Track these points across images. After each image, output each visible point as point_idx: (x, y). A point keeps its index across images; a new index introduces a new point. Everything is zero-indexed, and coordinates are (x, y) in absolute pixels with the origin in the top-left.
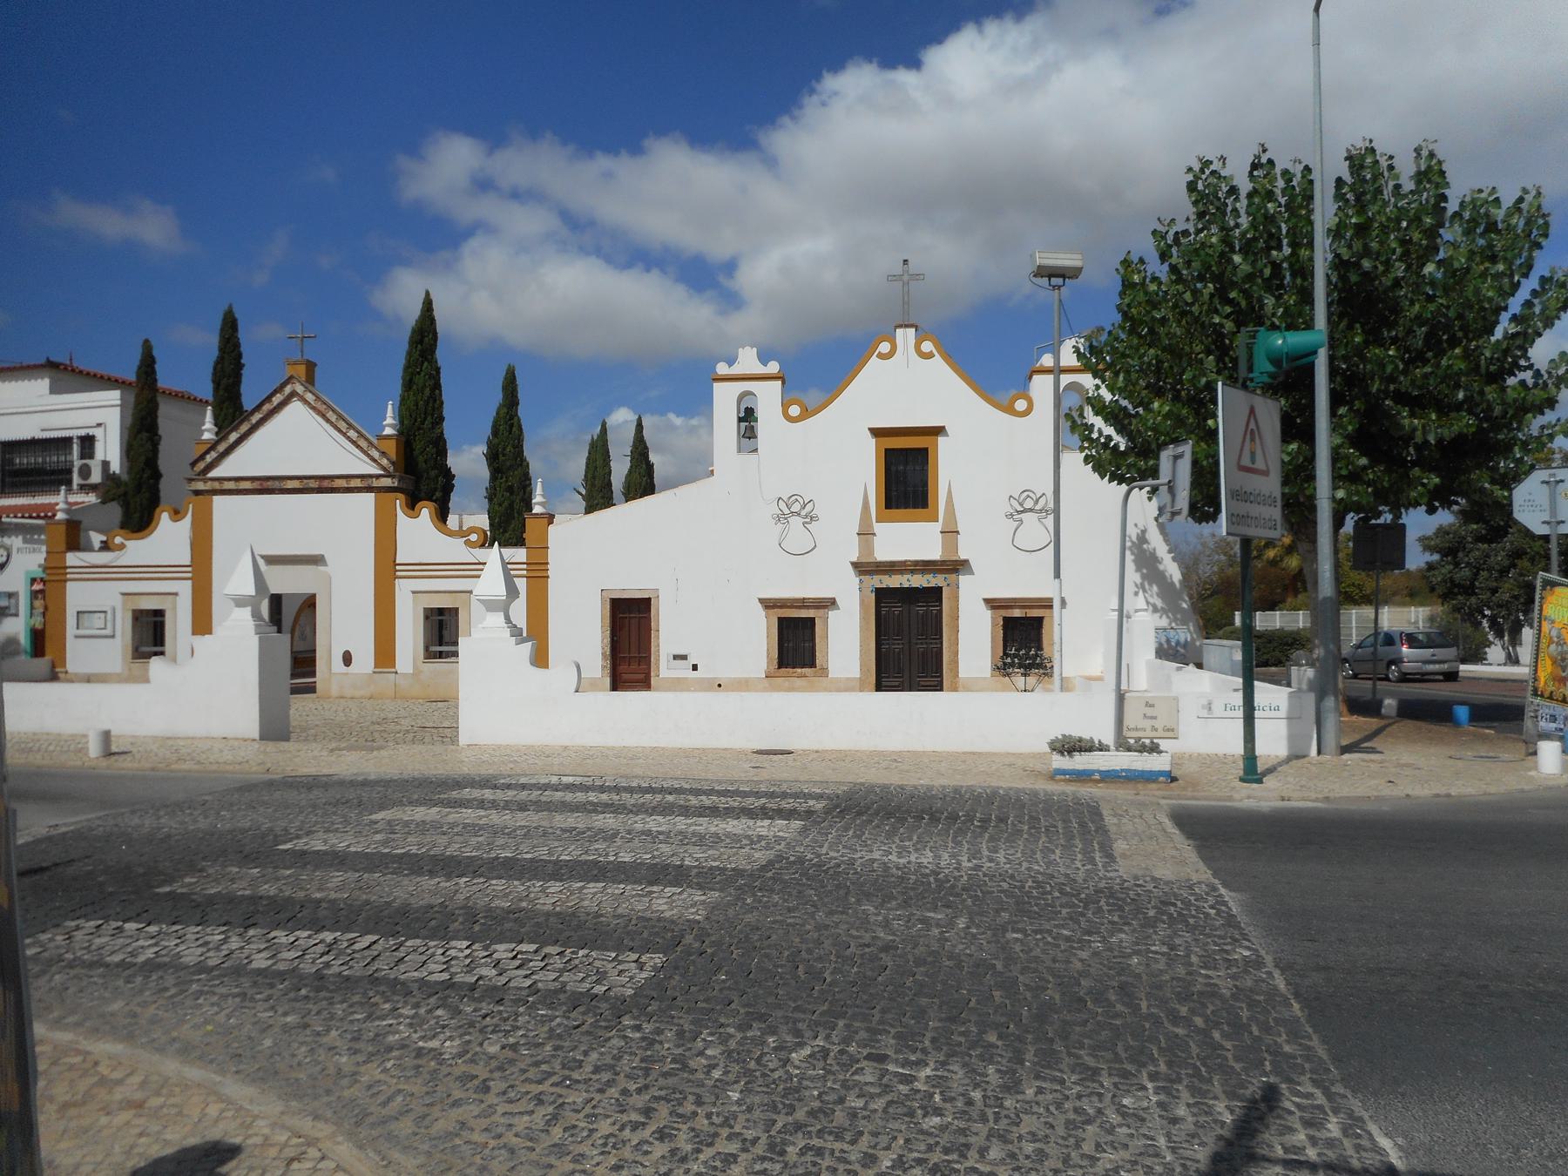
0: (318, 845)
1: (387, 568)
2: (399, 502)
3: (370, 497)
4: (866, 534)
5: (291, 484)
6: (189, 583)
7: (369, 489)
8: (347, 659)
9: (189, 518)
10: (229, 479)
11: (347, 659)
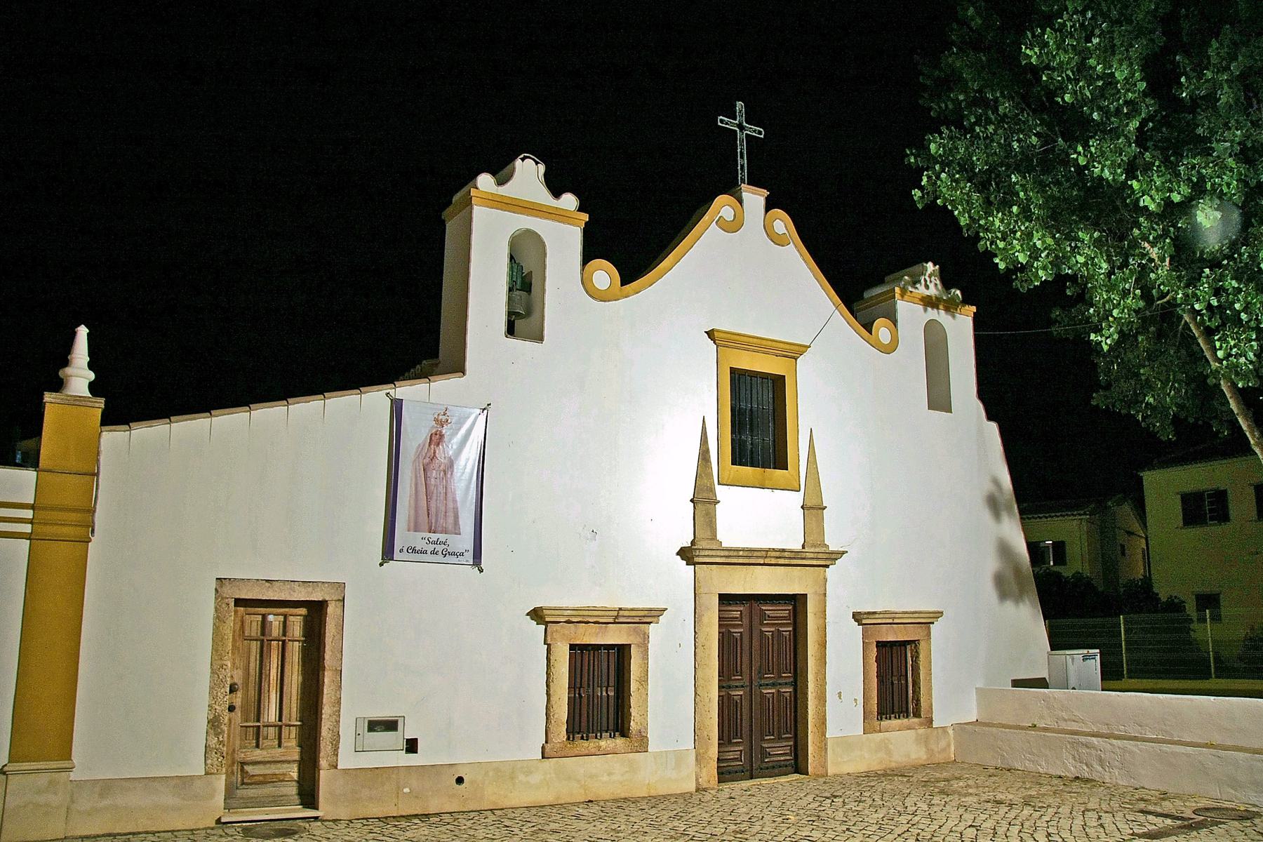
4: (703, 501)
6: (25, 544)
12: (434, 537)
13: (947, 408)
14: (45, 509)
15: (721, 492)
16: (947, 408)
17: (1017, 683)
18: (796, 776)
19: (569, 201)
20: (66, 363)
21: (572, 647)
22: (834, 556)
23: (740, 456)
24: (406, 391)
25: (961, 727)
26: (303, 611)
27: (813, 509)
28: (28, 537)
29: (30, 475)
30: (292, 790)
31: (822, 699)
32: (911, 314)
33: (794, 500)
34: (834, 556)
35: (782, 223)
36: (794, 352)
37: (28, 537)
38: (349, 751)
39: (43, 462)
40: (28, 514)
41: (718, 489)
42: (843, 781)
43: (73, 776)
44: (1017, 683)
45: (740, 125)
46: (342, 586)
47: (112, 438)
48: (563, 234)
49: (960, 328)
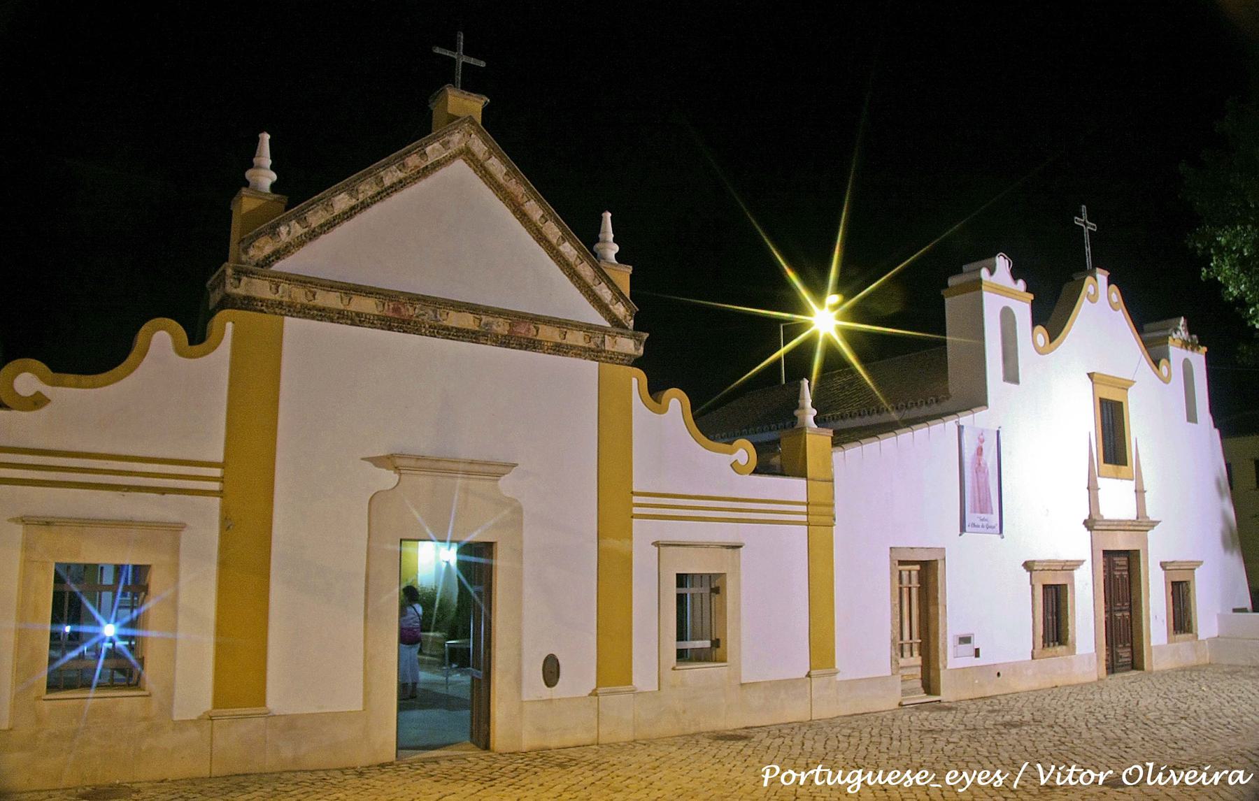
0: (528, 590)
1: (616, 502)
2: (637, 380)
3: (591, 367)
4: (1092, 488)
5: (455, 319)
6: (217, 501)
7: (595, 354)
8: (551, 671)
9: (224, 350)
10: (332, 286)
11: (551, 671)
12: (983, 516)
13: (1016, 381)
14: (815, 505)
15: (1101, 482)
16: (1016, 381)
17: (1235, 610)
18: (1134, 673)
19: (1021, 283)
20: (797, 406)
21: (1044, 586)
22: (1153, 524)
23: (1107, 460)
24: (965, 419)
25: (1211, 640)
26: (917, 567)
27: (1140, 492)
28: (219, 493)
29: (801, 483)
30: (918, 684)
31: (1148, 619)
32: (1177, 353)
33: (1130, 485)
34: (1153, 524)
35: (1116, 295)
36: (1125, 385)
37: (219, 493)
38: (953, 659)
39: (809, 475)
40: (217, 472)
41: (1099, 479)
42: (1164, 674)
43: (839, 677)
44: (1235, 610)
45: (1085, 224)
46: (943, 549)
47: (838, 455)
48: (1023, 311)
49: (1198, 359)
